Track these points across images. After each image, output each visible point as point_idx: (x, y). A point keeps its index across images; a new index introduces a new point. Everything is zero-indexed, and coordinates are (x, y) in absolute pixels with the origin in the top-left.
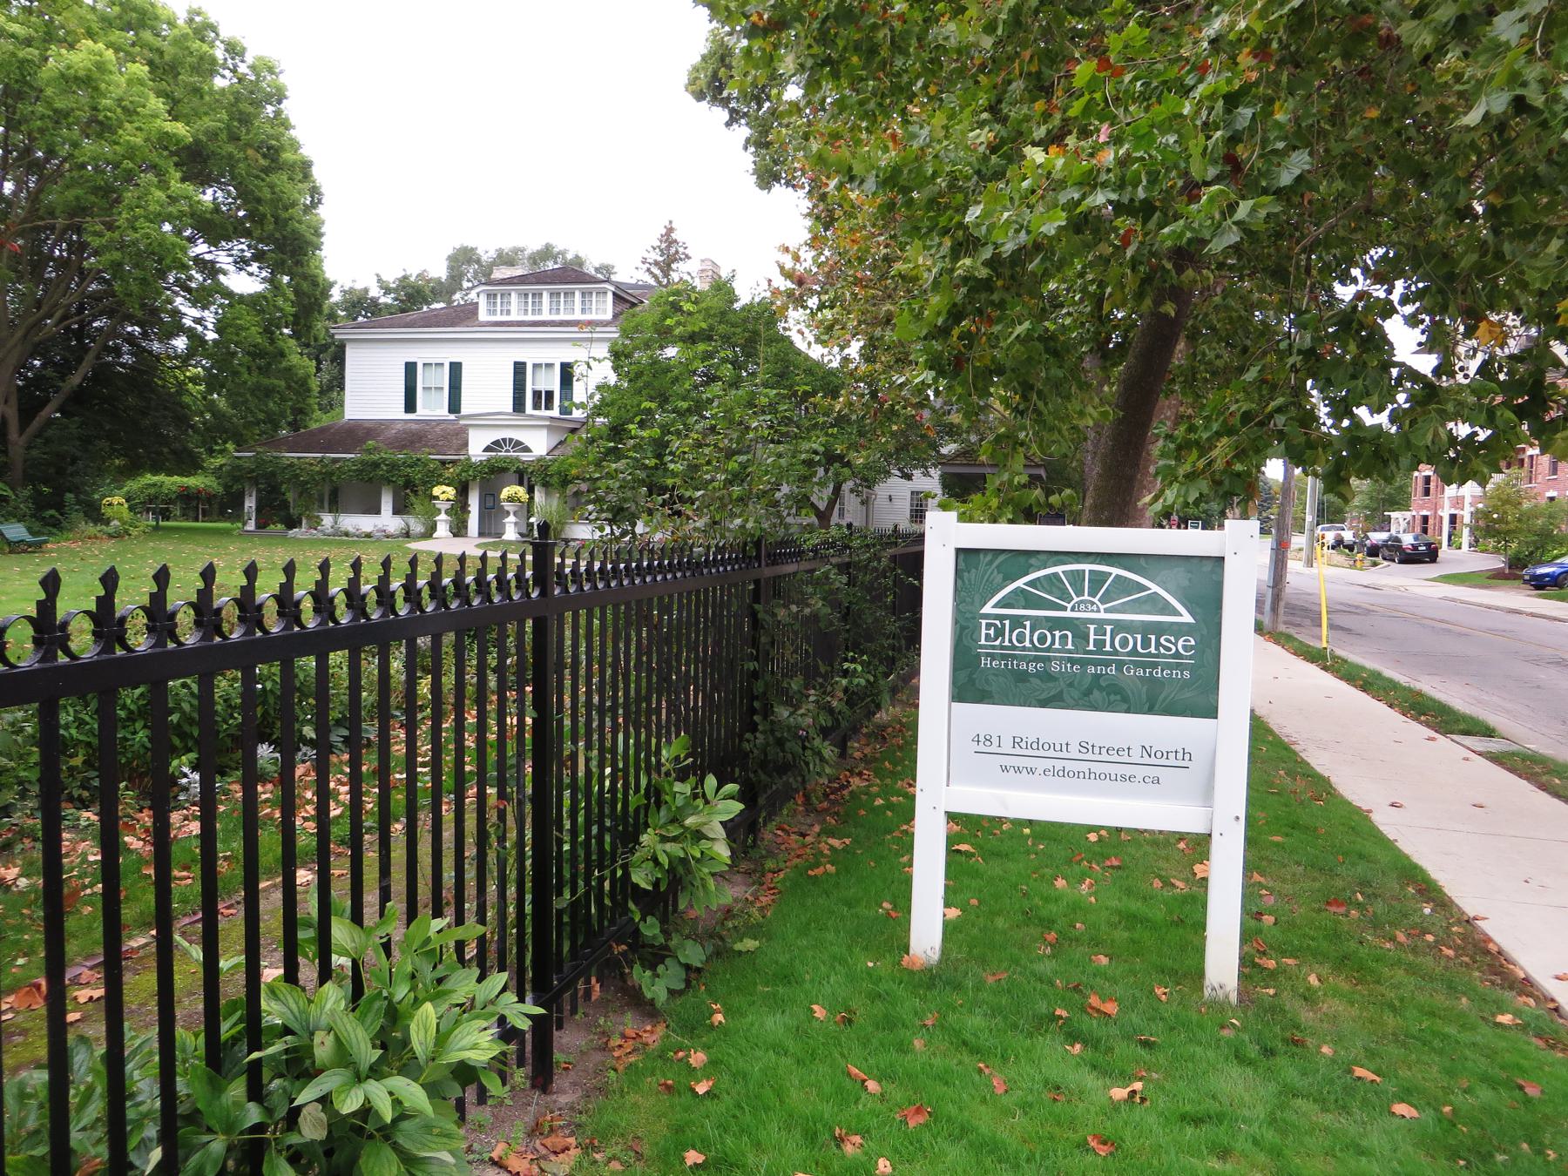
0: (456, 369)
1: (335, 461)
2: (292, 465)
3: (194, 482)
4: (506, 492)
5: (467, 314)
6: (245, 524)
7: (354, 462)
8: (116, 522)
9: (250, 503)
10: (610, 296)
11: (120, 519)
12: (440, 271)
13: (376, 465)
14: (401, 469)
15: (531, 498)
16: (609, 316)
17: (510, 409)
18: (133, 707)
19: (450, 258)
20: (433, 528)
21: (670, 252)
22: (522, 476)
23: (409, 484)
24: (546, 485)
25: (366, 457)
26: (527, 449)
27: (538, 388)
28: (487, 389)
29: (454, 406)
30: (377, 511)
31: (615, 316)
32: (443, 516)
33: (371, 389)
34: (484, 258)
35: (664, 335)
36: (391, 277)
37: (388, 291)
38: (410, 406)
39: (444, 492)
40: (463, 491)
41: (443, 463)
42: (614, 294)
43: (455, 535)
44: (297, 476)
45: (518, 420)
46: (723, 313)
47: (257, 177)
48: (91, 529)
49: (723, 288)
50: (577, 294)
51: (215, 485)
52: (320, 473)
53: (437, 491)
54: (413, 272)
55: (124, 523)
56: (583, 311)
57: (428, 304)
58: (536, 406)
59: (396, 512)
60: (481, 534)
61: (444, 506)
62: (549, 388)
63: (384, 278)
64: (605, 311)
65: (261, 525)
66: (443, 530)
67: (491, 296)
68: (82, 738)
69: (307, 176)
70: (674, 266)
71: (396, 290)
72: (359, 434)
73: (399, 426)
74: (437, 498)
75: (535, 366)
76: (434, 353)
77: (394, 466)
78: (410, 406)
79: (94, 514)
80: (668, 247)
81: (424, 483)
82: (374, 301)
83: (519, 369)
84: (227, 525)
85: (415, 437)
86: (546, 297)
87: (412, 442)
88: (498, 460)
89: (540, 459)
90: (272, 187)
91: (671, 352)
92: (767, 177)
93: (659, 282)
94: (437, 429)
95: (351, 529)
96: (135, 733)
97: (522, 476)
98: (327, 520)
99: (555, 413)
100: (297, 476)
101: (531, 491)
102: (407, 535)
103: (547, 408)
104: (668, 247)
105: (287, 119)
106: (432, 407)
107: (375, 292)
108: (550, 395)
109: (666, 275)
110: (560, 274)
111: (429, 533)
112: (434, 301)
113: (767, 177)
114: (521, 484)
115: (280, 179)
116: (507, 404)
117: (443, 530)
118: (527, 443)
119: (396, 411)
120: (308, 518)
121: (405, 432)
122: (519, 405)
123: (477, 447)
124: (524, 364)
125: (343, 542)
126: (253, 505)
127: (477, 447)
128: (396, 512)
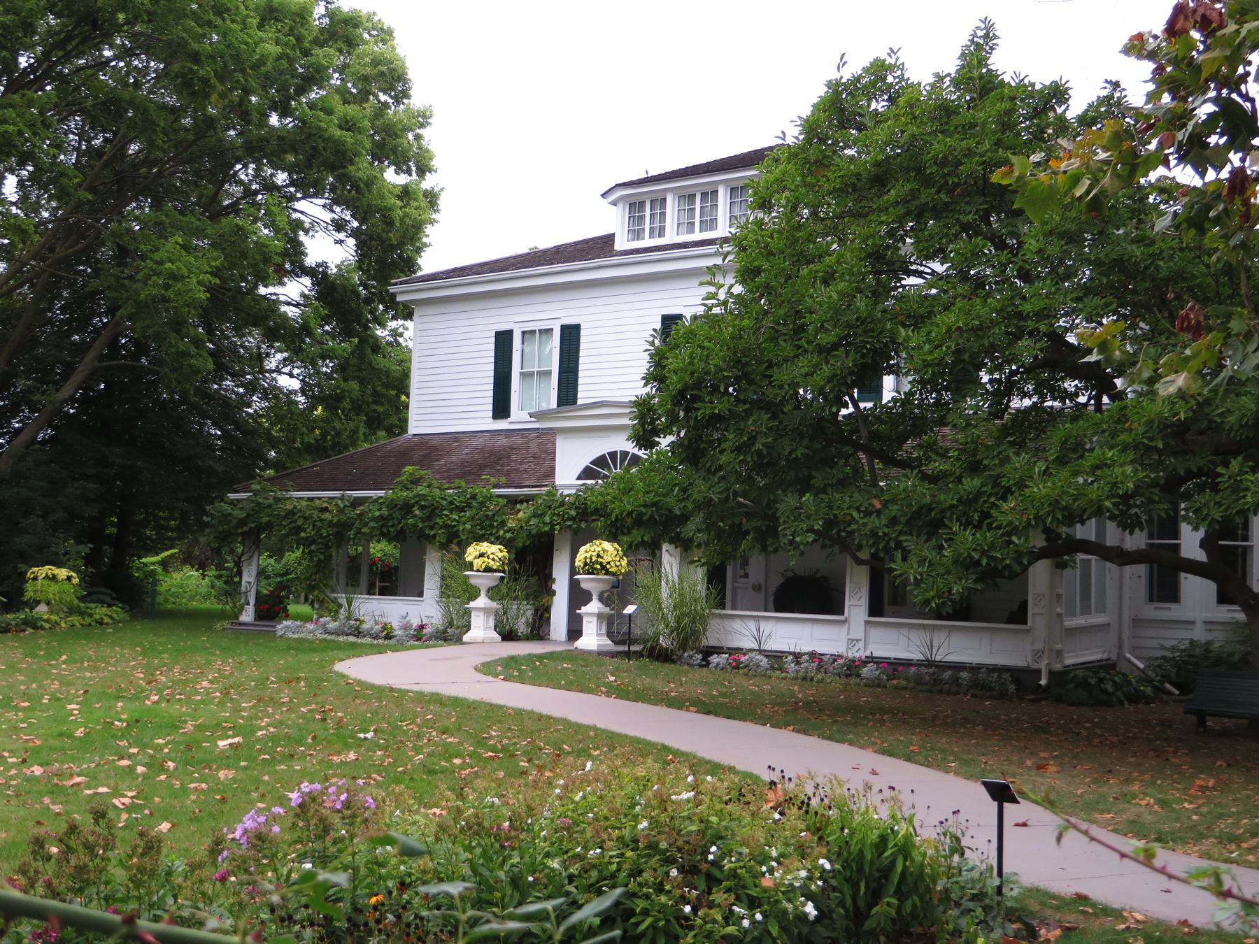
0: (571, 335)
1: (358, 502)
13: (407, 508)
32: (482, 601)
38: (501, 408)
39: (486, 554)
41: (513, 501)
72: (431, 449)
73: (478, 443)
74: (470, 566)
78: (501, 408)
121: (482, 451)
126: (252, 580)
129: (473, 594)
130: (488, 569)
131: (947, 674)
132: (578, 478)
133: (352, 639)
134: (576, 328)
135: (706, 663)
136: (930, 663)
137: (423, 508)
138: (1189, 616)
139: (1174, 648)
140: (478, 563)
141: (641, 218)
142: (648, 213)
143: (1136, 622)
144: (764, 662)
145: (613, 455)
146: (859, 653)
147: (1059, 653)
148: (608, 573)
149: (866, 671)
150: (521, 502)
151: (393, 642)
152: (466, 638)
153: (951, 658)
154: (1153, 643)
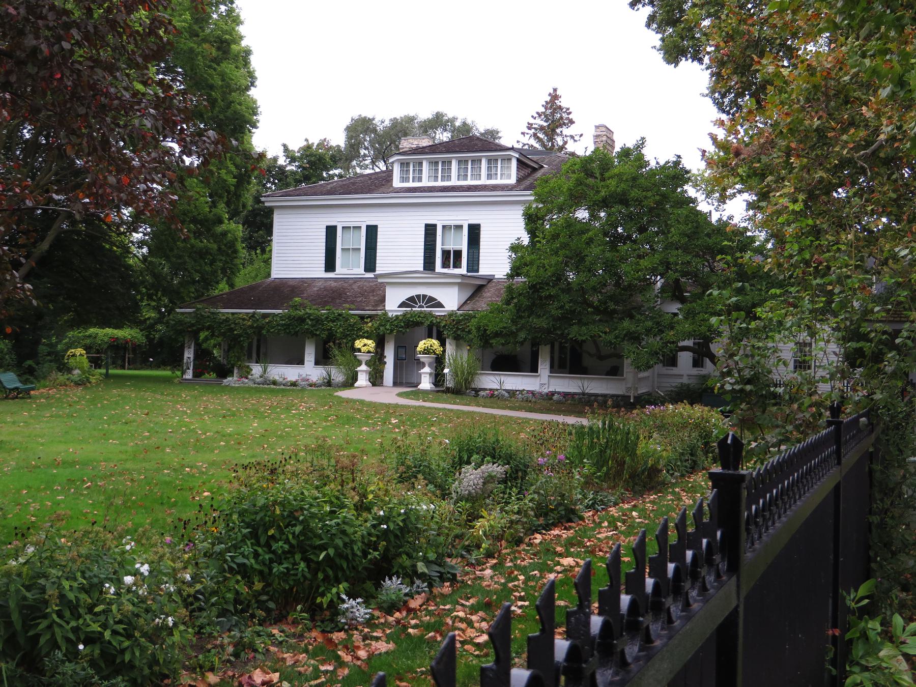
0: (372, 231)
1: (265, 316)
2: (227, 320)
3: (125, 333)
4: (422, 345)
5: (382, 182)
6: (183, 373)
7: (282, 317)
8: (77, 372)
9: (189, 354)
10: (514, 163)
11: (81, 369)
12: (339, 140)
13: (302, 320)
14: (328, 323)
15: (444, 351)
16: (513, 180)
17: (421, 268)
18: (294, 542)
19: (348, 129)
20: (355, 379)
21: (554, 117)
22: (437, 330)
23: (331, 337)
24: (457, 338)
25: (294, 313)
26: (440, 305)
27: (447, 247)
28: (401, 249)
29: (370, 265)
30: (300, 361)
31: (519, 180)
32: (363, 367)
33: (296, 250)
34: (380, 128)
35: (576, 199)
36: (296, 146)
37: (293, 159)
38: (330, 265)
39: (366, 345)
40: (380, 345)
41: (362, 317)
42: (518, 160)
43: (374, 384)
44: (232, 330)
45: (429, 278)
46: (634, 179)
47: (210, 67)
48: (62, 377)
49: (241, 38)
50: (484, 162)
51: (139, 336)
52: (251, 327)
53: (358, 344)
54: (315, 140)
55: (84, 372)
56: (489, 177)
57: (328, 170)
58: (445, 265)
59: (317, 363)
60: (395, 384)
61: (363, 357)
62: (457, 248)
63: (290, 148)
64: (509, 177)
65: (197, 374)
66: (363, 380)
67: (404, 165)
68: (256, 566)
69: (246, 63)
70: (558, 131)
71: (301, 158)
73: (319, 284)
74: (359, 350)
75: (444, 227)
76: (352, 218)
77: (318, 320)
78: (330, 265)
79: (64, 368)
80: (553, 114)
81: (346, 336)
82: (282, 169)
83: (430, 230)
84: (167, 373)
85: (336, 293)
86: (454, 165)
87: (333, 299)
88: (413, 314)
89: (451, 314)
90: (223, 76)
91: (582, 214)
92: (673, 53)
93: (543, 145)
94: (355, 287)
95: (277, 378)
96: (295, 564)
97: (437, 330)
98: (257, 370)
99: (463, 270)
100: (232, 330)
101: (443, 344)
102: (329, 383)
103: (455, 267)
104: (553, 114)
105: (238, 16)
106: (350, 267)
107: (282, 161)
108: (458, 254)
109: (551, 139)
110: (472, 144)
111: (350, 382)
112: (332, 168)
113: (673, 53)
114: (430, 336)
115: (227, 67)
116: (419, 265)
117: (363, 380)
118: (439, 299)
119: (317, 270)
120: (240, 368)
121: (325, 289)
122: (429, 264)
123: (393, 302)
124: (435, 226)
125: (272, 391)
126: (192, 356)
127: (393, 302)
128: (317, 363)
129: (360, 363)
130: (369, 352)
131: (593, 398)
132: (400, 306)
133: (272, 386)
134: (376, 227)
135: (477, 395)
136: (583, 394)
137: (311, 320)
138: (681, 373)
139: (676, 387)
140: (364, 349)
141: (408, 171)
142: (411, 169)
143: (659, 375)
144: (507, 394)
145: (418, 296)
146: (545, 390)
147: (636, 389)
148: (435, 354)
149: (556, 397)
150: (367, 318)
151: (298, 388)
152: (356, 385)
153: (592, 392)
154: (668, 385)
